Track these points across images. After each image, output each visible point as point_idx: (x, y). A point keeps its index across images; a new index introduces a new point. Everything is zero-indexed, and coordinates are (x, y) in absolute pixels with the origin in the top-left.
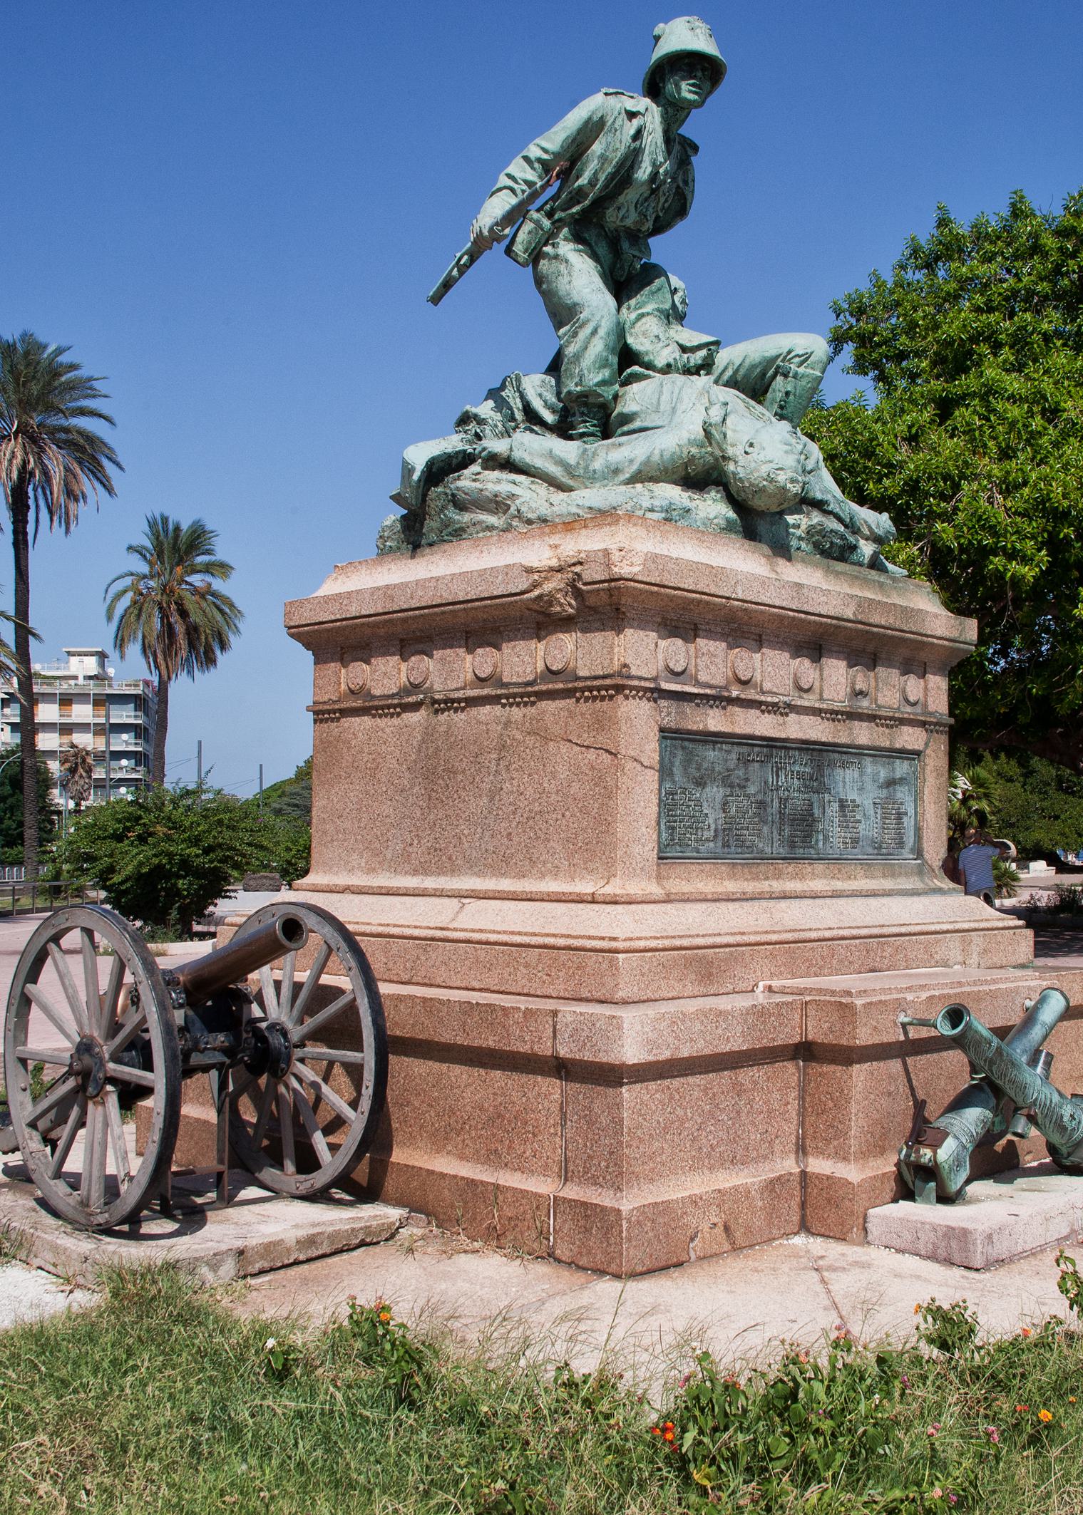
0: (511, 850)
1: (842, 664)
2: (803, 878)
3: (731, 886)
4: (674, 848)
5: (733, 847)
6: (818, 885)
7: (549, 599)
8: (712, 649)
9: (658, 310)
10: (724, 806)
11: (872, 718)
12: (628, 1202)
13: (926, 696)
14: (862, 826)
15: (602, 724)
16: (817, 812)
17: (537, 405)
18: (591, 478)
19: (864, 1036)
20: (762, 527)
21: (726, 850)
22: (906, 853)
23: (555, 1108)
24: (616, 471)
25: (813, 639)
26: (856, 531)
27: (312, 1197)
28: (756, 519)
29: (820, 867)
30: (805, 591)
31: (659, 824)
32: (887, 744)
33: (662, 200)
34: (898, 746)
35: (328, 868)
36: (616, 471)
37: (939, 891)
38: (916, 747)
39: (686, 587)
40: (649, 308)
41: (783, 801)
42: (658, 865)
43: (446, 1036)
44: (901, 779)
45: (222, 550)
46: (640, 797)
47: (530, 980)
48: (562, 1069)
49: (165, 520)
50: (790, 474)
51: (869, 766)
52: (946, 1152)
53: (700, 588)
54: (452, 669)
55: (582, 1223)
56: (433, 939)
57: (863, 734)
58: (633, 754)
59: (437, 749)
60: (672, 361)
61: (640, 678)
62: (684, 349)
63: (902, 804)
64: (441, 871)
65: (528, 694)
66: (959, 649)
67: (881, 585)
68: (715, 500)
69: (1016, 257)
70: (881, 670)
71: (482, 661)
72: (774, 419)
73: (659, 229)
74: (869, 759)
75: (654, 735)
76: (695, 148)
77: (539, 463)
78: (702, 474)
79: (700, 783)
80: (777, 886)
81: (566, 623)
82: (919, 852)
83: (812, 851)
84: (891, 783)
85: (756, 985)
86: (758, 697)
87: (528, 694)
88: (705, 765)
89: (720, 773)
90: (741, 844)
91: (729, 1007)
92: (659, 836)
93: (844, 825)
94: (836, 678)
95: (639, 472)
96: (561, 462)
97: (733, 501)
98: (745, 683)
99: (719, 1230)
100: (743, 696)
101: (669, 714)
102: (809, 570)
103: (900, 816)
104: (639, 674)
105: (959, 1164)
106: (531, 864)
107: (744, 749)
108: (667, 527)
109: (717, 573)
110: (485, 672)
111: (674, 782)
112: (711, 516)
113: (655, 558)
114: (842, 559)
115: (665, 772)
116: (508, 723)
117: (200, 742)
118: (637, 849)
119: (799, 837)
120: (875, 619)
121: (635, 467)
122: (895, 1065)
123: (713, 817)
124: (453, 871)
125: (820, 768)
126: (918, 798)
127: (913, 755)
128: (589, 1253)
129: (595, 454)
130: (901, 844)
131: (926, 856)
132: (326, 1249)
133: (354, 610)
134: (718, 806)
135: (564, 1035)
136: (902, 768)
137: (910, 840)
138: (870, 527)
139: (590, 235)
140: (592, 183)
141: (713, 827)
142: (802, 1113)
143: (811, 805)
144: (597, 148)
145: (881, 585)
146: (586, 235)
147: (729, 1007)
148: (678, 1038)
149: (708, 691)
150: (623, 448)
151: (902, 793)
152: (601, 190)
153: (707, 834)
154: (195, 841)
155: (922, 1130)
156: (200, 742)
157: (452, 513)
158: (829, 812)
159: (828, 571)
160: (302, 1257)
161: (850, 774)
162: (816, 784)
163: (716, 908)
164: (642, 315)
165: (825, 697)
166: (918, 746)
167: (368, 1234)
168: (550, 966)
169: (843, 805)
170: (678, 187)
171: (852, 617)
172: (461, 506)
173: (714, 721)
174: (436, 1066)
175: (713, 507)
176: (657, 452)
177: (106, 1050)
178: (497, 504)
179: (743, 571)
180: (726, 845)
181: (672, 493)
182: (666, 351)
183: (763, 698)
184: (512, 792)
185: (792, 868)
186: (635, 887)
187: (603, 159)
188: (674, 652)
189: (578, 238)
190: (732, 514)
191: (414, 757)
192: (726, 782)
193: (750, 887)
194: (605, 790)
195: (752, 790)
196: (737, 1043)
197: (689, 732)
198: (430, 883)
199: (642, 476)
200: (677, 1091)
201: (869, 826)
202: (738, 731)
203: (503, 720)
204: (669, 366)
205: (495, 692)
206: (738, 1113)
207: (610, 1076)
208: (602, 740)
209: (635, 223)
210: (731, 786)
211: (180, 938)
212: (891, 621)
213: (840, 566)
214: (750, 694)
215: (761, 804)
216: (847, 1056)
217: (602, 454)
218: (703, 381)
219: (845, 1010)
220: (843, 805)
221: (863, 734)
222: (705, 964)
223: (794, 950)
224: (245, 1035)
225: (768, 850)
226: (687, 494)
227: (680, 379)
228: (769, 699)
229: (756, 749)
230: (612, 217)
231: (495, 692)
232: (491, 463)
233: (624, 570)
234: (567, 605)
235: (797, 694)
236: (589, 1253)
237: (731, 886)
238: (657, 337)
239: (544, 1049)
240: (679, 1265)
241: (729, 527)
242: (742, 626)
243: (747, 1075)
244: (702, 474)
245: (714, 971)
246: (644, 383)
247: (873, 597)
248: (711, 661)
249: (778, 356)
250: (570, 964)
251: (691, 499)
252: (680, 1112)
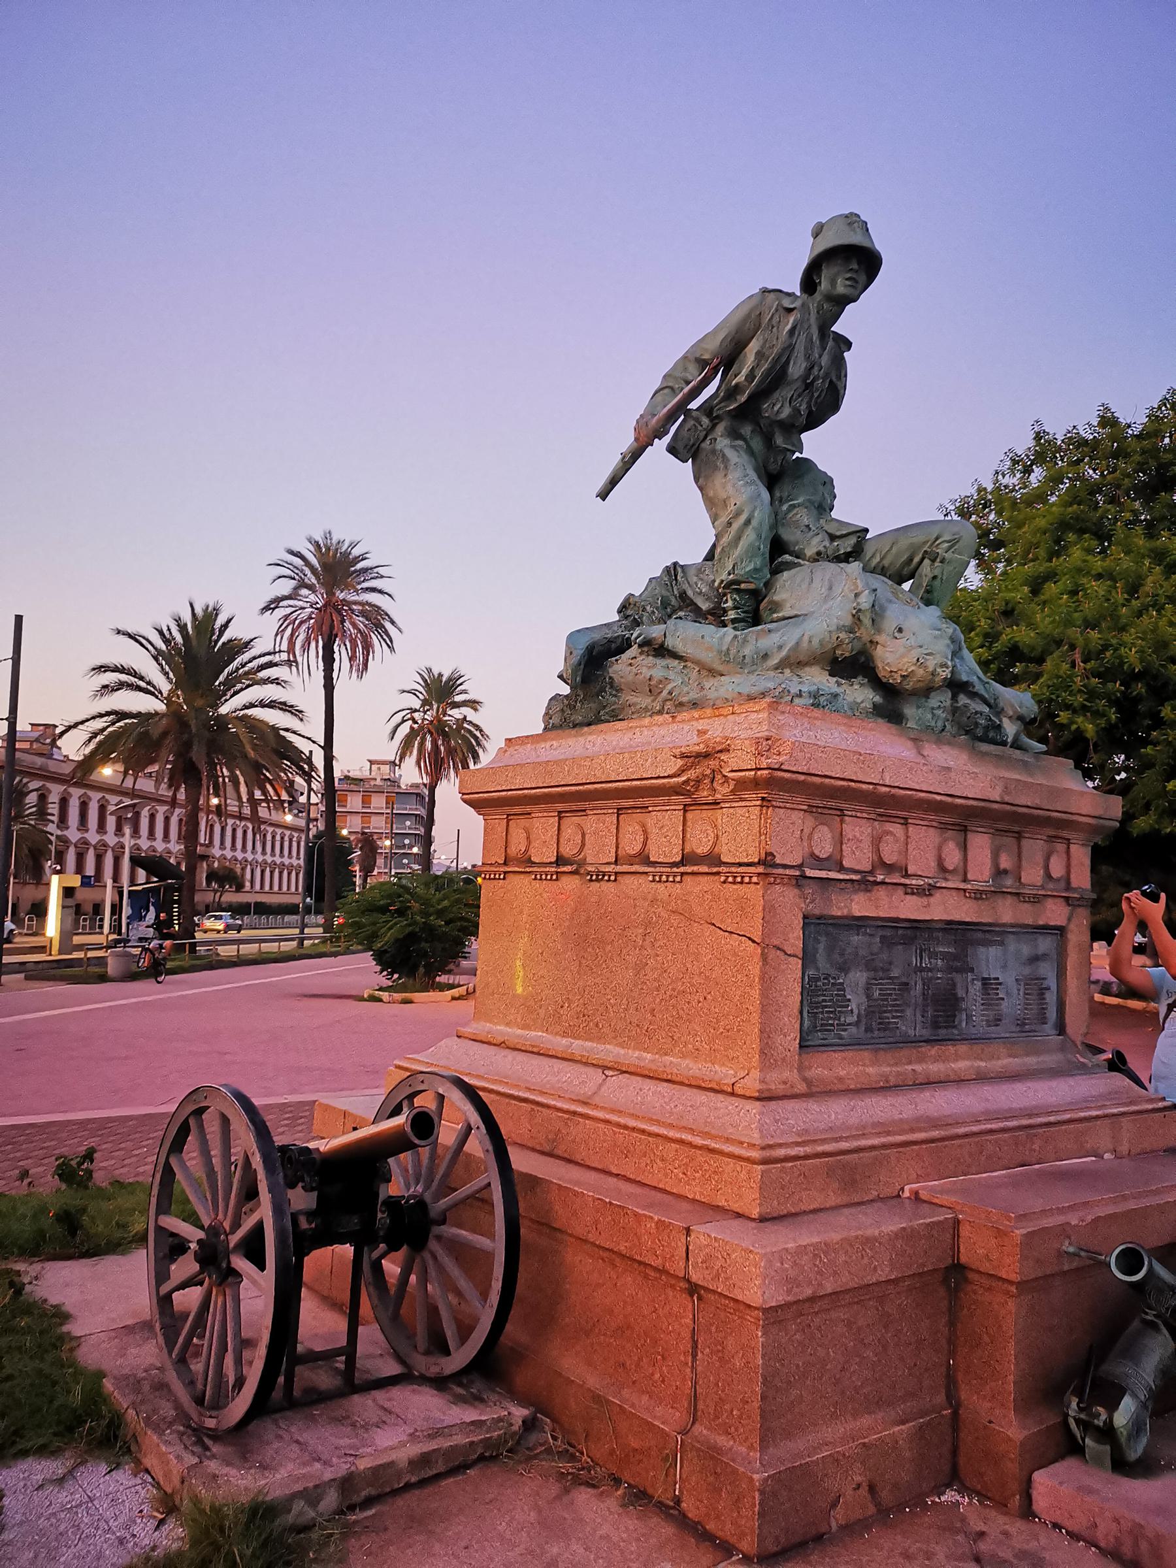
2: (946, 1060)
5: (879, 1032)
8: (858, 835)
9: (809, 501)
13: (1068, 872)
14: (1004, 1004)
16: (961, 993)
21: (869, 1035)
22: (1049, 1028)
23: (686, 1334)
26: (999, 712)
27: (440, 1383)
29: (963, 1048)
30: (953, 774)
31: (801, 1013)
32: (1030, 921)
33: (816, 395)
34: (1041, 923)
36: (766, 656)
38: (1059, 923)
39: (833, 775)
40: (800, 500)
41: (926, 983)
42: (800, 1055)
44: (1044, 955)
45: (472, 689)
47: (666, 1175)
49: (429, 670)
50: (939, 659)
51: (1012, 945)
53: (846, 775)
55: (711, 1479)
56: (574, 1113)
58: (776, 942)
59: (588, 919)
60: (822, 549)
61: (785, 866)
62: (833, 538)
63: (1044, 979)
66: (1103, 827)
67: (1025, 764)
68: (862, 685)
72: (922, 605)
73: (814, 420)
74: (1011, 937)
75: (798, 922)
76: (848, 345)
79: (844, 969)
82: (1061, 1029)
83: (956, 1032)
84: (1035, 959)
85: (902, 1189)
86: (903, 881)
88: (849, 950)
89: (864, 957)
91: (877, 1233)
92: (801, 1025)
93: (987, 1005)
95: (787, 658)
99: (864, 1491)
100: (887, 880)
101: (812, 901)
102: (954, 752)
103: (1042, 991)
104: (785, 862)
107: (888, 933)
108: (817, 713)
111: (818, 969)
112: (859, 701)
114: (984, 739)
115: (808, 958)
116: (654, 901)
117: (604, 495)
118: (779, 1039)
119: (944, 1016)
121: (784, 653)
123: (856, 1002)
127: (1061, 931)
128: (718, 1517)
129: (745, 641)
130: (1043, 1020)
131: (1069, 1030)
132: (441, 1467)
134: (861, 991)
135: (696, 1258)
136: (1045, 944)
137: (1052, 1014)
138: (1012, 706)
139: (747, 430)
141: (856, 1011)
143: (954, 985)
144: (753, 347)
145: (1025, 764)
146: (743, 432)
147: (877, 1233)
148: (820, 1273)
149: (854, 877)
150: (773, 635)
152: (757, 386)
153: (849, 1019)
154: (440, 913)
156: (604, 495)
158: (971, 990)
160: (414, 1479)
161: (993, 952)
162: (960, 964)
164: (794, 506)
165: (969, 876)
167: (486, 1448)
168: (686, 1165)
170: (831, 381)
171: (998, 799)
173: (859, 906)
175: (860, 694)
176: (806, 638)
180: (869, 1029)
181: (819, 679)
182: (816, 540)
183: (907, 881)
184: (653, 969)
185: (934, 1051)
189: (734, 434)
190: (878, 699)
191: (567, 924)
192: (869, 966)
195: (895, 973)
197: (834, 918)
198: (578, 1046)
199: (794, 663)
200: (819, 1328)
201: (1012, 1003)
202: (882, 914)
203: (650, 897)
204: (819, 553)
206: (885, 1347)
209: (790, 416)
210: (875, 970)
211: (425, 989)
212: (1038, 801)
213: (985, 747)
217: (752, 638)
218: (855, 567)
220: (986, 982)
221: (1007, 912)
224: (379, 1215)
225: (911, 1032)
226: (835, 679)
227: (832, 567)
228: (914, 882)
229: (900, 932)
232: (646, 649)
236: (718, 1517)
238: (808, 526)
240: (819, 1538)
242: (888, 805)
244: (853, 664)
245: (858, 1177)
246: (793, 571)
247: (1018, 777)
248: (858, 841)
249: (925, 543)
250: (706, 1167)
251: (839, 684)
252: (821, 1352)
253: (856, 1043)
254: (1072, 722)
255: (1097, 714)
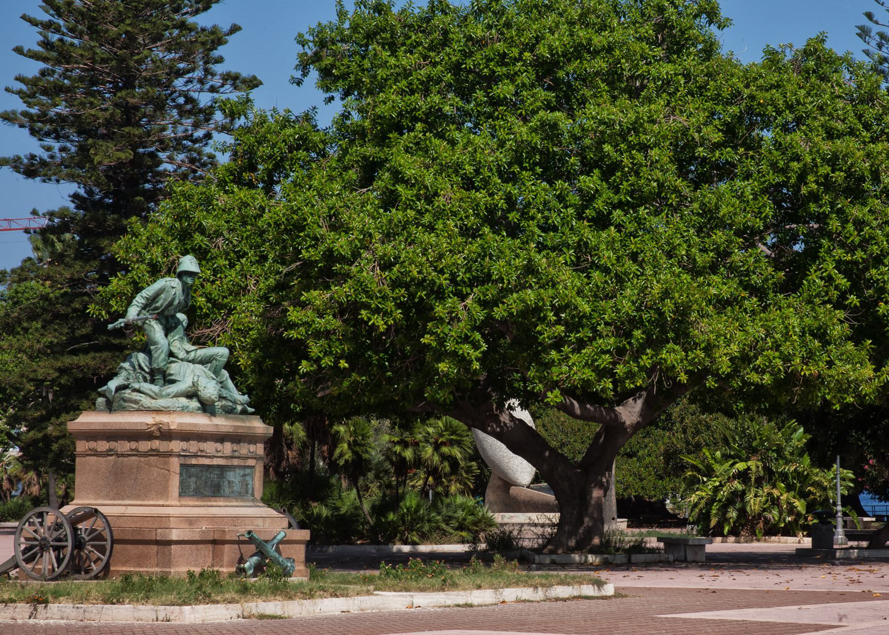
0: (141, 492)
1: (230, 444)
3: (197, 503)
4: (183, 493)
5: (198, 494)
6: (221, 504)
7: (152, 432)
10: (196, 483)
11: (238, 458)
12: (172, 570)
15: (166, 463)
17: (143, 365)
18: (162, 397)
19: (228, 538)
20: (208, 408)
24: (169, 395)
25: (221, 438)
28: (207, 407)
29: (222, 499)
35: (81, 498)
37: (259, 506)
43: (127, 538)
46: (175, 482)
48: (157, 543)
51: (237, 471)
52: (247, 565)
54: (124, 446)
57: (236, 462)
64: (119, 499)
65: (146, 454)
69: (431, 48)
70: (242, 444)
71: (133, 445)
77: (148, 392)
78: (192, 395)
79: (190, 477)
80: (209, 503)
81: (157, 438)
82: (253, 495)
84: (244, 475)
87: (146, 454)
90: (200, 493)
93: (229, 488)
94: (228, 447)
96: (153, 392)
97: (200, 401)
98: (202, 451)
103: (247, 485)
105: (250, 569)
106: (146, 497)
109: (195, 425)
110: (133, 447)
113: (180, 424)
115: (181, 475)
120: (239, 431)
122: (236, 546)
123: (193, 486)
124: (123, 499)
125: (222, 472)
126: (253, 479)
130: (247, 493)
133: (93, 428)
136: (248, 471)
140: (162, 305)
142: (213, 557)
151: (248, 478)
155: (241, 560)
157: (122, 402)
159: (226, 418)
161: (232, 473)
162: (221, 476)
163: (194, 508)
166: (253, 464)
169: (229, 482)
172: (125, 401)
173: (194, 461)
174: (123, 546)
175: (194, 404)
177: (50, 539)
178: (136, 402)
179: (202, 422)
181: (183, 401)
186: (173, 503)
187: (165, 300)
188: (183, 445)
192: (196, 477)
193: (202, 504)
194: (167, 480)
196: (197, 538)
198: (116, 502)
199: (177, 396)
201: (237, 488)
205: (137, 453)
207: (170, 543)
208: (166, 467)
213: (230, 416)
214: (203, 454)
215: (205, 482)
216: (224, 542)
219: (223, 532)
220: (229, 482)
221: (236, 462)
222: (190, 521)
223: (213, 518)
230: (166, 313)
231: (137, 453)
233: (172, 427)
234: (158, 434)
235: (215, 453)
237: (197, 503)
239: (153, 538)
241: (199, 409)
243: (200, 546)
244: (192, 395)
248: (193, 446)
253: (192, 496)
254: (370, 319)
255: (386, 314)
